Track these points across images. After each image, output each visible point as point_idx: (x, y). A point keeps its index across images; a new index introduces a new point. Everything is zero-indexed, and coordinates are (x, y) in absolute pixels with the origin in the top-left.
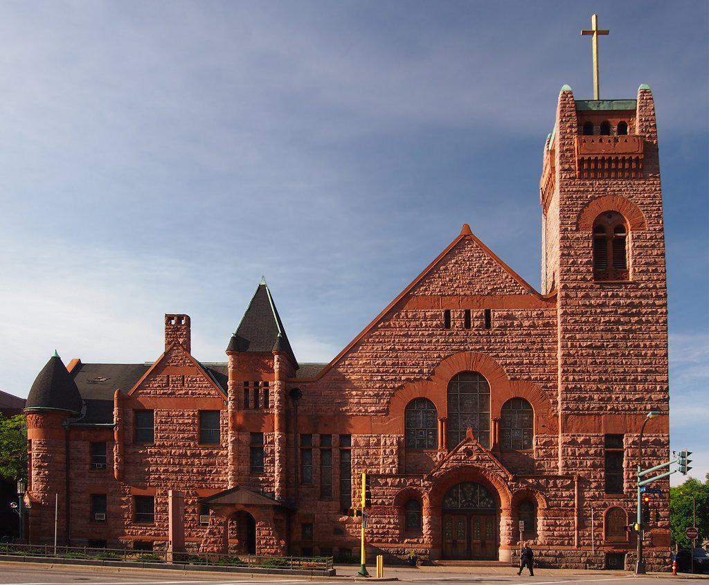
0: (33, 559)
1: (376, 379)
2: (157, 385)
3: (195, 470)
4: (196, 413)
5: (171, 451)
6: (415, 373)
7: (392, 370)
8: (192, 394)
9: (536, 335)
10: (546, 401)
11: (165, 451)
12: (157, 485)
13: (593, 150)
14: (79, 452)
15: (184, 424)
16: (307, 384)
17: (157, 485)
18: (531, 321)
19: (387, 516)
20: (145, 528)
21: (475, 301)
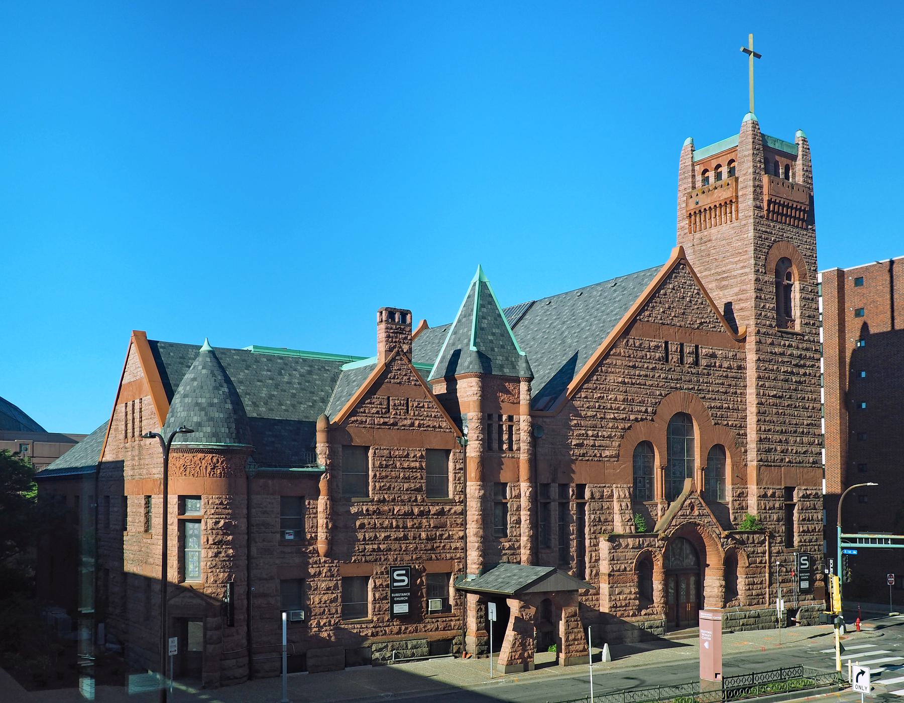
0: (801, 693)
1: (608, 417)
2: (374, 410)
3: (423, 535)
4: (424, 453)
5: (394, 510)
6: (641, 412)
7: (623, 407)
8: (419, 426)
9: (732, 378)
10: (739, 450)
11: (386, 508)
12: (376, 560)
13: (778, 193)
14: (265, 512)
15: (409, 468)
16: (547, 420)
17: (376, 560)
18: (728, 363)
19: (628, 584)
20: (359, 626)
21: (687, 334)
